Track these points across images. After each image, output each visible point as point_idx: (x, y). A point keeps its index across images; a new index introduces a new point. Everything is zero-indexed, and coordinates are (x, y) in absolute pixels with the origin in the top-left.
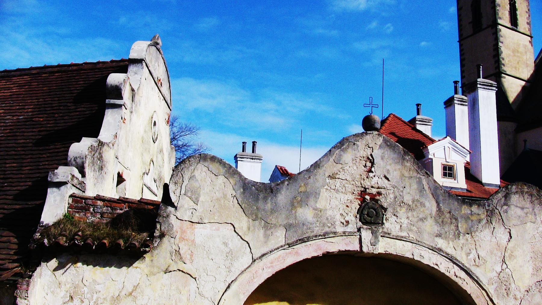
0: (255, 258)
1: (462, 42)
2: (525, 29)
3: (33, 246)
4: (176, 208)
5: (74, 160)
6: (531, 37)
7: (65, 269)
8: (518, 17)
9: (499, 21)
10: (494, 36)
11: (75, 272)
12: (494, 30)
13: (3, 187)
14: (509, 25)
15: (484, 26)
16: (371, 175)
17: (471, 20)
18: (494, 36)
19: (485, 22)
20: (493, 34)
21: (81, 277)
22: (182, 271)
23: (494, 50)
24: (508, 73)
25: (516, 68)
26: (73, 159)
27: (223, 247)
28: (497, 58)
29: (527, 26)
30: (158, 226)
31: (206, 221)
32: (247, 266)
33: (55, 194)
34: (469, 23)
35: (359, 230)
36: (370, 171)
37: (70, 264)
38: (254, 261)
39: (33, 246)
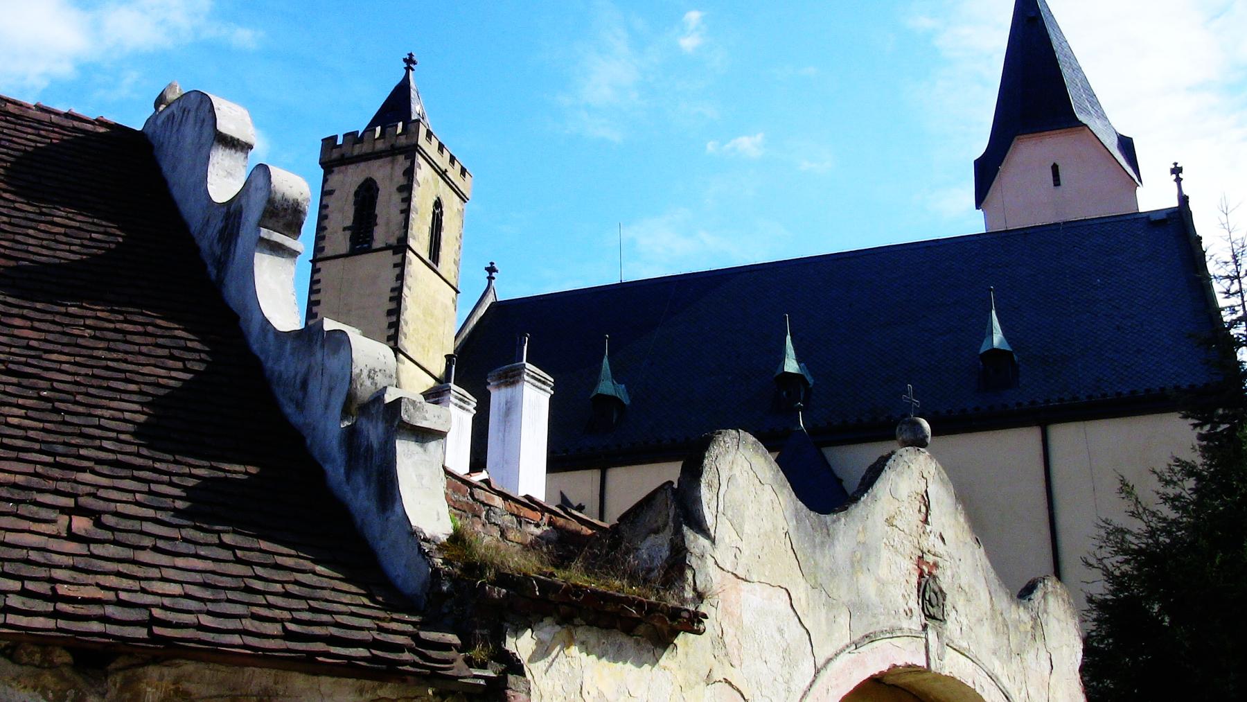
0: (819, 666)
1: (319, 265)
2: (449, 271)
3: (499, 592)
4: (713, 541)
5: (369, 377)
6: (457, 292)
7: (550, 659)
8: (442, 244)
9: (411, 243)
10: (397, 270)
11: (566, 669)
12: (398, 258)
13: (5, 393)
14: (426, 257)
15: (375, 245)
16: (928, 528)
17: (349, 223)
18: (397, 270)
19: (381, 236)
20: (395, 266)
21: (579, 681)
22: (730, 684)
23: (391, 299)
24: (409, 354)
25: (423, 348)
26: (365, 373)
27: (777, 636)
28: (394, 319)
29: (453, 267)
30: (689, 574)
31: (755, 578)
32: (808, 683)
33: (416, 457)
34: (345, 229)
35: (925, 627)
36: (926, 521)
37: (558, 648)
38: (817, 672)
39: (499, 592)
